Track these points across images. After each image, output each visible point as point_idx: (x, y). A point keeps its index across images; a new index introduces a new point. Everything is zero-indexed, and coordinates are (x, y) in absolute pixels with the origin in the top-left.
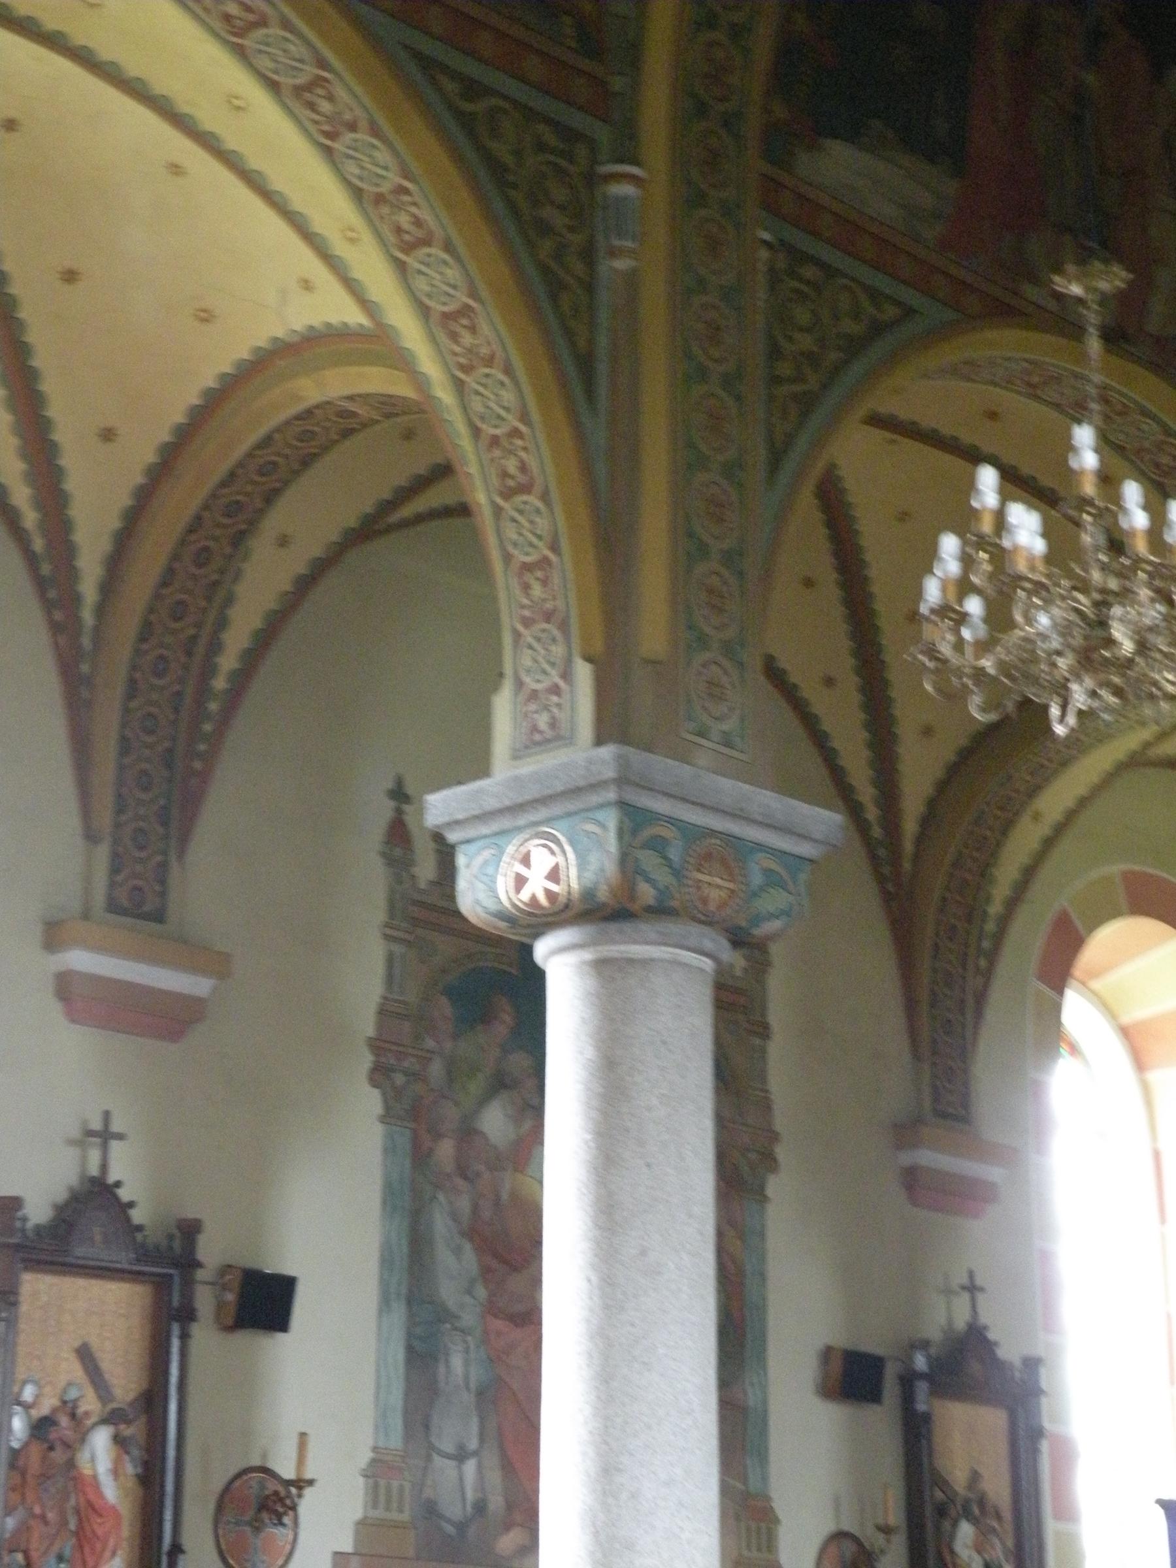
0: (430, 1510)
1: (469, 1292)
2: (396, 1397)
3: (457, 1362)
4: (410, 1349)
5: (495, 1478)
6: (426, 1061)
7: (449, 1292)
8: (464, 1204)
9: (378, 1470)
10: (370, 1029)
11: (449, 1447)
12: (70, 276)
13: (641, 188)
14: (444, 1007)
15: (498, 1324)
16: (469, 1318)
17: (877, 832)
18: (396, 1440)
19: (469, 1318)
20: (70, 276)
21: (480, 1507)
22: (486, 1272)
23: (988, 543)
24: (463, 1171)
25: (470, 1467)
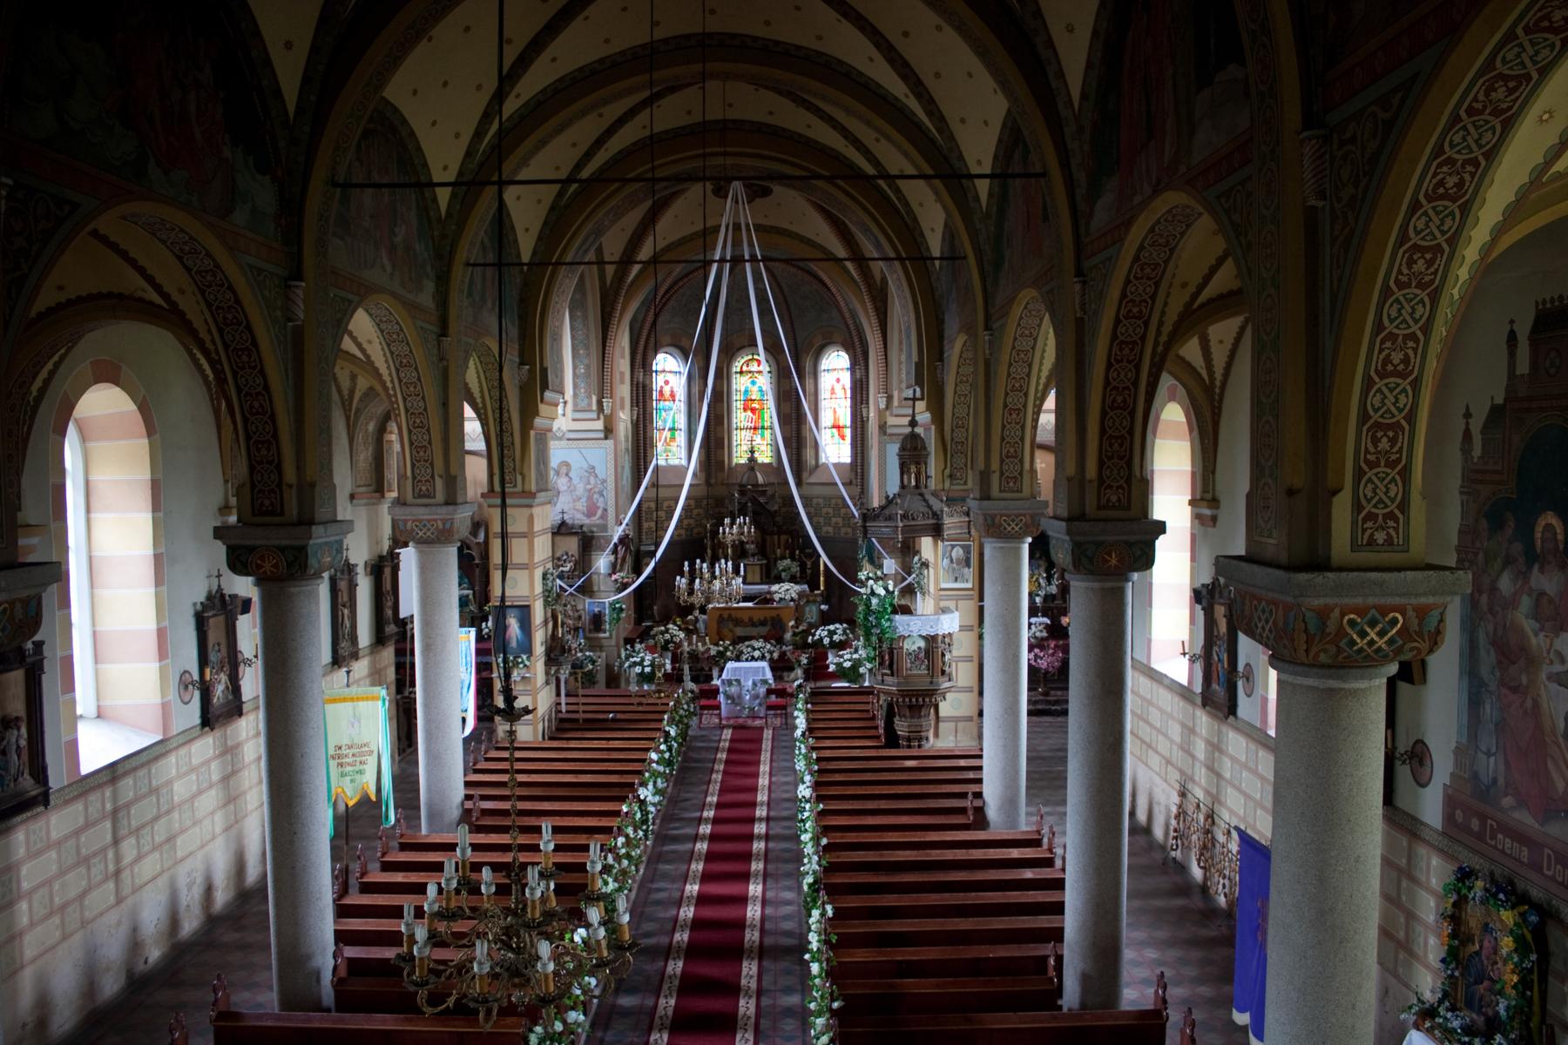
0: (1475, 776)
1: (1492, 673)
2: (1465, 721)
3: (1488, 707)
4: (1470, 699)
5: (1502, 768)
6: (1476, 554)
7: (1484, 672)
8: (1491, 627)
9: (1459, 751)
10: (1455, 542)
11: (1484, 749)
12: (415, 92)
13: (1346, 686)
14: (1484, 524)
15: (1504, 691)
16: (1493, 687)
17: (1160, 348)
18: (1464, 741)
19: (1493, 687)
20: (415, 92)
21: (1495, 781)
22: (1499, 662)
23: (480, 969)
24: (1490, 610)
25: (1492, 759)
